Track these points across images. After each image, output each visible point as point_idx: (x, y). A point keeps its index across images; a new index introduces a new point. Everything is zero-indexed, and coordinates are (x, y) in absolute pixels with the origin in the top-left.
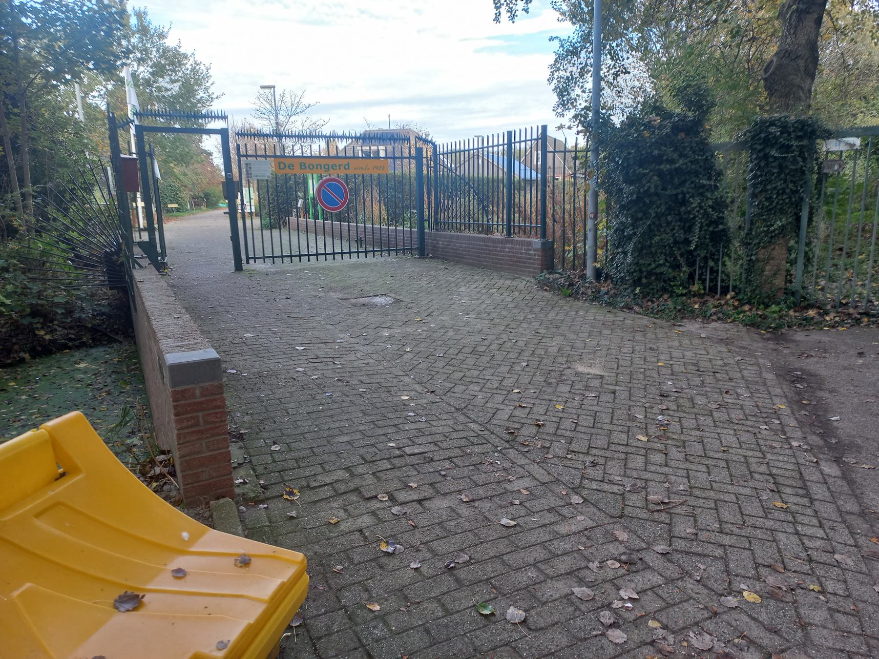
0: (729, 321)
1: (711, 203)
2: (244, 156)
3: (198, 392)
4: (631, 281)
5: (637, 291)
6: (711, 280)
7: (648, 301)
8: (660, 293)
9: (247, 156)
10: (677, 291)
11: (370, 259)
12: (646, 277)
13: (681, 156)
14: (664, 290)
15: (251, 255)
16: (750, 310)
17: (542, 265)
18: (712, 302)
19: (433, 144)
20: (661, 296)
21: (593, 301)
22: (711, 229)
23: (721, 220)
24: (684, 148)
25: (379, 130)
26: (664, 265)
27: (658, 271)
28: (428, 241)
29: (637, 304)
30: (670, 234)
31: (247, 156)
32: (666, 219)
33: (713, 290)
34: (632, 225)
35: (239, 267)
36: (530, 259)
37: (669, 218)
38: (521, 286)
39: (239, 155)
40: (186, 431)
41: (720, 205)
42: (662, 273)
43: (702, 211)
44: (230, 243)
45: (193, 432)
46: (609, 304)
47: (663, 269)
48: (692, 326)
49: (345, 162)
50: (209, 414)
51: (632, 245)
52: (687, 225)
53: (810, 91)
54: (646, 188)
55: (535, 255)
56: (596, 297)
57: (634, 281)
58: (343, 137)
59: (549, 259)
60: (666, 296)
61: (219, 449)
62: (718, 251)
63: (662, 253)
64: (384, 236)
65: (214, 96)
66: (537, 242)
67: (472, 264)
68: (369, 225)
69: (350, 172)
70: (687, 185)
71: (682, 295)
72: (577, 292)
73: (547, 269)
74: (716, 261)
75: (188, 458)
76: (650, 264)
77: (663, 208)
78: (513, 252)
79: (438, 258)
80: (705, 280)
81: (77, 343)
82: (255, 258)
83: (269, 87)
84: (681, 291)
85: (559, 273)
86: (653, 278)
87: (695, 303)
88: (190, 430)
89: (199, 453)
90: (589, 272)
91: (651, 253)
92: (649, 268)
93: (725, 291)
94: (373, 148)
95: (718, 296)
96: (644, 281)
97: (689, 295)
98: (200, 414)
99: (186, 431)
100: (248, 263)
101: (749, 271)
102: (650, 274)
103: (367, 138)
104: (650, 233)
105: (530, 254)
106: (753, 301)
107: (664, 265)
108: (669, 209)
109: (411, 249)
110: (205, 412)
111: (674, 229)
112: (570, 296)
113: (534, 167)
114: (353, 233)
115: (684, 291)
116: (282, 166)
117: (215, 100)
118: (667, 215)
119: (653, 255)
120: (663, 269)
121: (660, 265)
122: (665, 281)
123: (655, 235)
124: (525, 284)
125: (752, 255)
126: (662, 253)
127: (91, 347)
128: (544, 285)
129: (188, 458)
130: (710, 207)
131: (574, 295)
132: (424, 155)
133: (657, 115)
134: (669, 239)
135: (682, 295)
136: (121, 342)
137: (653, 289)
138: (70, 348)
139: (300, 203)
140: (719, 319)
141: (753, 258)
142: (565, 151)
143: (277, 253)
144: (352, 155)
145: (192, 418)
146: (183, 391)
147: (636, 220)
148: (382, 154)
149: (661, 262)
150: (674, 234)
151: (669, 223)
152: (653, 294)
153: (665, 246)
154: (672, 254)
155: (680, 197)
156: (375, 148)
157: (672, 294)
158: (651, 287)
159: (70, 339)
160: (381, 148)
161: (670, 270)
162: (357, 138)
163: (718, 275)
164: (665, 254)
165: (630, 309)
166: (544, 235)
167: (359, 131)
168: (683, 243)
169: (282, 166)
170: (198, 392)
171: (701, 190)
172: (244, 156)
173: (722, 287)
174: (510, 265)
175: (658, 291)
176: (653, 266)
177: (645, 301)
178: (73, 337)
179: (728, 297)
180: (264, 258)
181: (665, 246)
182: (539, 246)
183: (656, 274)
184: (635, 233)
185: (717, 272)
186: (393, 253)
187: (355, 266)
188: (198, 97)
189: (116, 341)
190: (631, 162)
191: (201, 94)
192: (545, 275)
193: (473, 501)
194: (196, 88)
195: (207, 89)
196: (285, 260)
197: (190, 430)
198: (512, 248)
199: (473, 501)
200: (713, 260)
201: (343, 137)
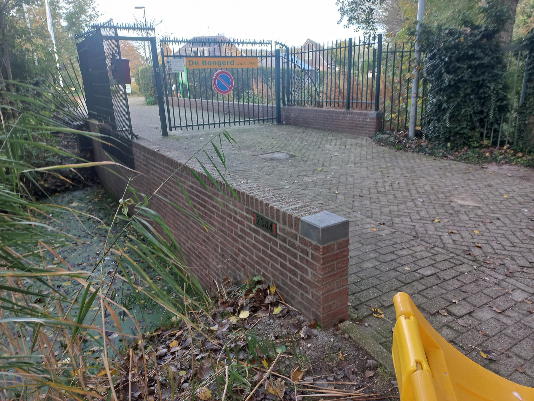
0: (513, 164)
1: (501, 86)
2: (166, 56)
3: (336, 247)
4: (443, 139)
5: (449, 145)
6: (494, 137)
7: (455, 151)
8: (462, 146)
9: (168, 56)
10: (473, 145)
11: (247, 126)
12: (453, 136)
13: (487, 55)
14: (464, 144)
15: (173, 125)
16: (523, 156)
17: (376, 128)
18: (496, 152)
19: (286, 47)
20: (463, 147)
21: (418, 152)
22: (498, 104)
23: (504, 98)
24: (486, 49)
25: (203, 37)
26: (466, 128)
27: (462, 132)
28: (283, 113)
29: (450, 154)
30: (472, 107)
31: (168, 56)
32: (470, 98)
33: (494, 144)
34: (446, 101)
35: (165, 134)
36: (367, 125)
37: (472, 97)
38: (364, 142)
39: (163, 57)
40: (327, 275)
41: (506, 88)
42: (464, 133)
43: (495, 92)
44: (159, 117)
45: (330, 276)
46: (430, 154)
47: (465, 131)
48: (493, 168)
49: (230, 60)
50: (339, 262)
51: (448, 115)
52: (482, 101)
53: (515, 11)
54: (460, 77)
55: (371, 122)
56: (420, 149)
57: (446, 138)
58: (175, 41)
59: (380, 125)
60: (466, 148)
61: (343, 286)
62: (500, 118)
63: (465, 120)
64: (246, 110)
65: (99, 13)
66: (373, 113)
67: (318, 129)
68: (261, 105)
69: (234, 67)
70: (486, 74)
71: (476, 147)
72: (405, 146)
73: (379, 131)
74: (499, 125)
75: (326, 295)
76: (456, 127)
77: (469, 91)
78: (352, 120)
79: (290, 124)
80: (490, 137)
81: (63, 188)
82: (175, 127)
83: (141, 8)
84: (476, 144)
85: (388, 134)
86: (458, 136)
87: (486, 152)
88: (329, 274)
89: (332, 290)
90: (411, 133)
91: (458, 120)
92: (456, 130)
93: (502, 144)
94: (199, 49)
95: (498, 147)
96: (452, 138)
97: (481, 146)
98: (335, 262)
99: (327, 275)
100: (171, 130)
101: (520, 131)
102: (456, 133)
103: (196, 42)
104: (458, 107)
105: (366, 122)
106: (524, 150)
107: (466, 128)
108: (473, 91)
109: (272, 119)
110: (338, 261)
111: (473, 104)
112: (401, 149)
113: (307, 61)
114: (216, 107)
115: (478, 145)
116: (191, 63)
117: (100, 17)
118: (470, 95)
119: (459, 121)
120: (465, 131)
121: (463, 128)
122: (465, 138)
123: (462, 109)
124: (364, 141)
125: (525, 120)
126: (465, 120)
127: (72, 191)
128: (380, 142)
129: (326, 295)
130: (501, 89)
131: (405, 149)
132: (281, 55)
133: (467, 26)
134: (470, 110)
135: (476, 147)
136: (91, 186)
137: (457, 144)
138: (59, 192)
139: (174, 87)
140: (506, 162)
141: (527, 122)
142: (324, 50)
143: (184, 124)
144: (230, 55)
145: (331, 266)
146: (328, 247)
147: (449, 98)
148: (206, 54)
149: (465, 126)
150: (474, 107)
151: (471, 100)
152: (457, 147)
153: (467, 116)
154: (471, 121)
155: (481, 82)
156: (202, 49)
157: (470, 147)
158: (456, 142)
159: (58, 186)
160: (206, 49)
161: (470, 131)
162: (189, 42)
163: (498, 134)
164: (467, 121)
165: (446, 157)
166: (377, 109)
167: (190, 37)
168: (478, 113)
169: (191, 63)
170: (336, 247)
171: (495, 78)
172: (166, 56)
173: (501, 141)
174: (354, 129)
175: (460, 145)
176: (458, 128)
177: (453, 151)
178: (59, 184)
179: (505, 147)
180: (181, 127)
181: (467, 116)
182: (375, 116)
183: (460, 134)
184: (449, 107)
185: (498, 132)
186: (261, 122)
187: (244, 131)
188: (88, 14)
189: (88, 186)
190: (453, 59)
191: (90, 11)
192: (380, 136)
193: (503, 311)
194: (87, 7)
195: (94, 9)
196: (189, 128)
197: (329, 274)
198: (352, 118)
199: (503, 311)
200: (497, 123)
201: (175, 41)
